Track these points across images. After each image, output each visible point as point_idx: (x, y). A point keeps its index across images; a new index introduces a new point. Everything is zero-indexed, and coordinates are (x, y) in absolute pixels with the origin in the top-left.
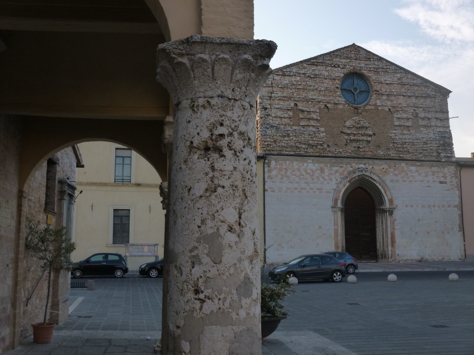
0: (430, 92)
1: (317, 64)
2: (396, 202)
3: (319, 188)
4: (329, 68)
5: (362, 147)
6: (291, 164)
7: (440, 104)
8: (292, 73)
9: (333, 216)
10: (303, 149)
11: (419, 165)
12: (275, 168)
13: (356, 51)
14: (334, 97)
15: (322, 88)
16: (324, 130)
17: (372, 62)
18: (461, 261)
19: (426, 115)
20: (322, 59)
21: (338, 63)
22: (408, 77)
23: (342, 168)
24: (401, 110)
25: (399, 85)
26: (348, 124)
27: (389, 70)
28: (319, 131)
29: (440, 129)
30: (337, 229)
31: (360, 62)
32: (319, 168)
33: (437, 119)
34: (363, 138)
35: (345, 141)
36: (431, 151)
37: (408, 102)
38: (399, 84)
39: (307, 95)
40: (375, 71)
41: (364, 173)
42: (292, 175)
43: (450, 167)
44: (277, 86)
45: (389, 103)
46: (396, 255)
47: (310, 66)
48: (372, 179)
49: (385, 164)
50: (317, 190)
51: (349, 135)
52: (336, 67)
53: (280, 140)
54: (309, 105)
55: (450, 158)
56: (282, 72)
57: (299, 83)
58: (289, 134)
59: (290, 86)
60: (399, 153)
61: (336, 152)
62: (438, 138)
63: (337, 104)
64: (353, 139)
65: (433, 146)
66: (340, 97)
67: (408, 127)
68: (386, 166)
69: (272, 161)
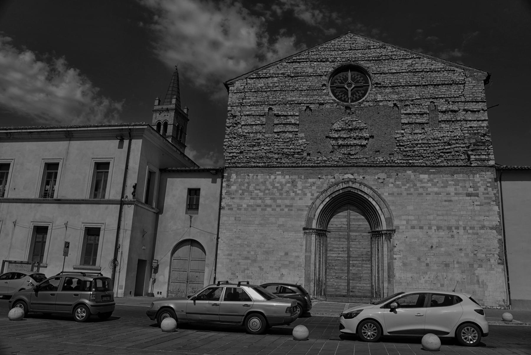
1: (300, 61)
3: (289, 204)
4: (315, 63)
5: (353, 153)
6: (255, 177)
7: (472, 91)
8: (268, 74)
10: (275, 159)
11: (434, 172)
13: (352, 40)
14: (319, 95)
15: (304, 87)
18: (502, 308)
19: (450, 107)
20: (307, 55)
21: (326, 57)
22: (424, 62)
23: (321, 180)
24: (412, 104)
25: (410, 74)
26: (336, 126)
27: (395, 56)
29: (471, 124)
30: (310, 257)
32: (290, 180)
34: (355, 142)
35: (331, 147)
36: (457, 154)
37: (423, 93)
38: (410, 71)
43: (484, 173)
44: (249, 91)
45: (395, 97)
50: (285, 207)
51: (336, 139)
53: (248, 151)
56: (256, 75)
57: (277, 85)
59: (265, 89)
60: (407, 158)
61: (319, 162)
62: (467, 136)
64: (341, 144)
65: (460, 146)
68: (383, 176)
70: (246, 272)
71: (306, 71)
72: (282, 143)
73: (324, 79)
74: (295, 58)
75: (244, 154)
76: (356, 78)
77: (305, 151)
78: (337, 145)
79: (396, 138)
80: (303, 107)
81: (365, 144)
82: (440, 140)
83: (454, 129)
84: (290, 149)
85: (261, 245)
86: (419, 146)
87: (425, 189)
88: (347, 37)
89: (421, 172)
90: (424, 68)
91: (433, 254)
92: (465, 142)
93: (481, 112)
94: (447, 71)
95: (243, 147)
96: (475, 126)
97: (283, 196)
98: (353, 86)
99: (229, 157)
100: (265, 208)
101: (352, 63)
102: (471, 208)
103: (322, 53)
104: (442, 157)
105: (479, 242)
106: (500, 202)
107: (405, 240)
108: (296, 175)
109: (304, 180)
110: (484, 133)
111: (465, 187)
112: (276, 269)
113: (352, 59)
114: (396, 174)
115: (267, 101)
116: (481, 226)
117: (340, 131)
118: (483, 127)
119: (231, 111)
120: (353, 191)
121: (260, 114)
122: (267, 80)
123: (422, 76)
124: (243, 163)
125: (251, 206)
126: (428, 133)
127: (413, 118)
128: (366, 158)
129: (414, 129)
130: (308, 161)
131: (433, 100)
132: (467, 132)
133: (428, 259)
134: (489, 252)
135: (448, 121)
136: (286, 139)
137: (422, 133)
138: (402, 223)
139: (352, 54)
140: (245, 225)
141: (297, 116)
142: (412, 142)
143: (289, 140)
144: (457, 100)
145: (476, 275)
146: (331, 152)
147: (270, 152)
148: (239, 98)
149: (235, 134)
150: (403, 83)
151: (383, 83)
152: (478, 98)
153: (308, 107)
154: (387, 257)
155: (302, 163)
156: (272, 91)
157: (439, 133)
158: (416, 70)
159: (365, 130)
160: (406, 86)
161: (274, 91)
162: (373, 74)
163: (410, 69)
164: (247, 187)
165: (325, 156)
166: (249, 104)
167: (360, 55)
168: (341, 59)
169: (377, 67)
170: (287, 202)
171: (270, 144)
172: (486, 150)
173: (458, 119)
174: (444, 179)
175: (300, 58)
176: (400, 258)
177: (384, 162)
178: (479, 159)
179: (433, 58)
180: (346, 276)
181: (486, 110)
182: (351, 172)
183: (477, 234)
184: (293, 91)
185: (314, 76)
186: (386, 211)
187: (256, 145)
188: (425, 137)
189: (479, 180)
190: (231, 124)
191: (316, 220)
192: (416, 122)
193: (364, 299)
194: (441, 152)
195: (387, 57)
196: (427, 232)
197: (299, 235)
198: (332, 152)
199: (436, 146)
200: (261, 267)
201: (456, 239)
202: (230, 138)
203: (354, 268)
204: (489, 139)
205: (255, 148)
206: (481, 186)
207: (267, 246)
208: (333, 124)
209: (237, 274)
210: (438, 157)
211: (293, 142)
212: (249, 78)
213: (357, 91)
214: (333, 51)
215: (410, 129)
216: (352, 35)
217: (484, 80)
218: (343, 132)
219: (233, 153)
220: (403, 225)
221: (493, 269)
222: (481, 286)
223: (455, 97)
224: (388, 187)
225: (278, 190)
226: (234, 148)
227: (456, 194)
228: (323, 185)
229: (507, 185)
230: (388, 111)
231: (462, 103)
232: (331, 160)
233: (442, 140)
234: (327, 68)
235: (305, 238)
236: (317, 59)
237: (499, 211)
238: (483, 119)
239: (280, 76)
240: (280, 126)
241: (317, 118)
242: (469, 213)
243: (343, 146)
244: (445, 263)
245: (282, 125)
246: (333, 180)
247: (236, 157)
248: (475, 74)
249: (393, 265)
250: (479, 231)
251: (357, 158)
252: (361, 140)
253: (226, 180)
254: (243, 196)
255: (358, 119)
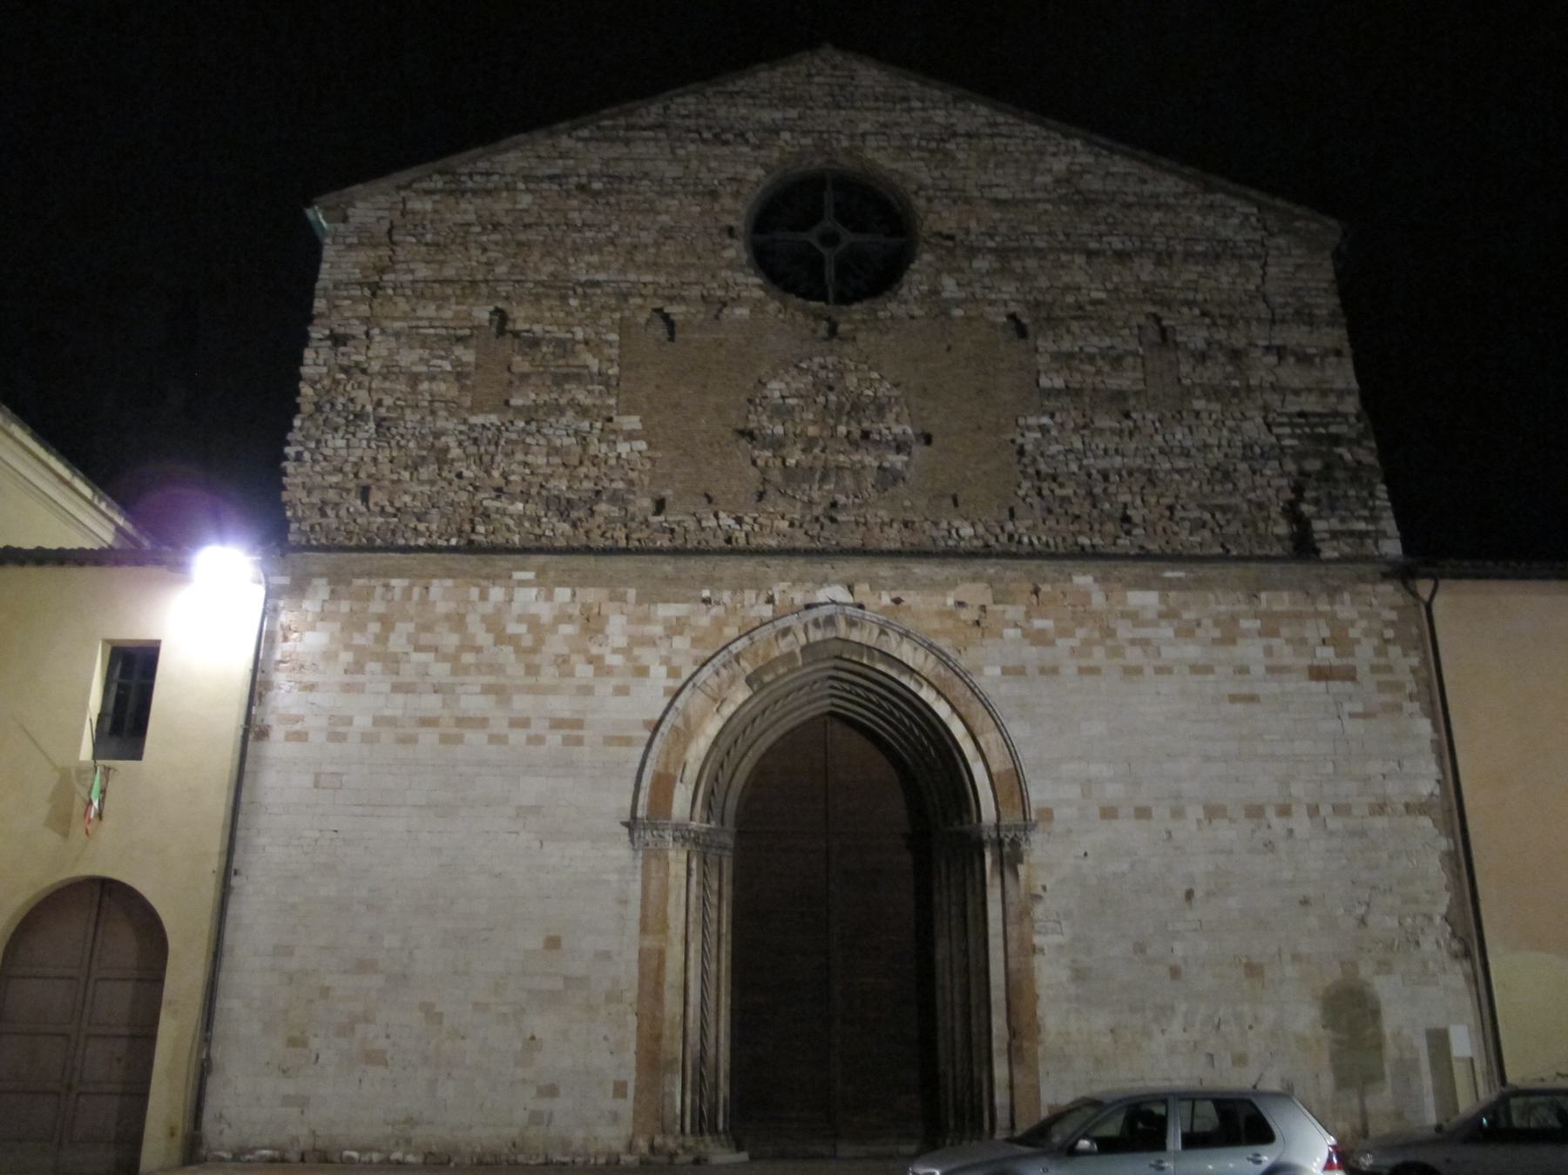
0: (1236, 233)
2: (1038, 794)
4: (692, 148)
9: (639, 877)
11: (1179, 579)
16: (639, 426)
22: (1114, 169)
25: (1064, 208)
28: (614, 431)
30: (661, 954)
31: (852, 113)
32: (575, 611)
33: (1281, 352)
39: (562, 269)
40: (932, 151)
41: (842, 630)
43: (1369, 588)
45: (1009, 289)
47: (592, 145)
48: (891, 666)
49: (975, 579)
52: (726, 143)
54: (568, 314)
55: (1369, 542)
58: (447, 450)
62: (1292, 447)
66: (741, 268)
67: (1120, 396)
68: (976, 593)
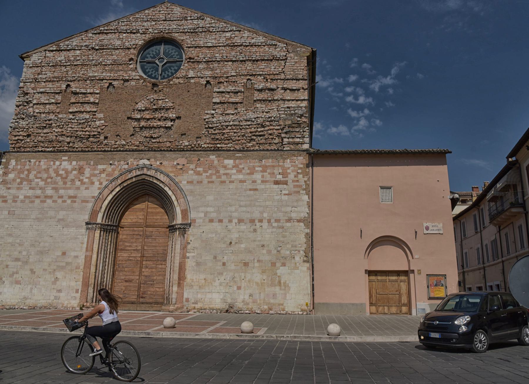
1: (107, 32)
3: (73, 195)
4: (124, 35)
5: (156, 136)
6: (37, 163)
7: (293, 68)
10: (66, 143)
11: (240, 156)
12: (13, 170)
13: (168, 10)
15: (108, 61)
17: (189, 21)
20: (116, 25)
22: (244, 35)
23: (112, 166)
24: (227, 82)
25: (227, 48)
26: (140, 106)
27: (213, 28)
29: (289, 104)
32: (77, 167)
34: (159, 124)
35: (132, 129)
37: (240, 69)
38: (228, 45)
41: (145, 171)
42: (36, 178)
43: (296, 158)
44: (47, 65)
45: (208, 73)
46: (184, 300)
48: (158, 181)
50: (68, 198)
51: (138, 120)
53: (37, 133)
56: (57, 47)
57: (78, 58)
59: (64, 63)
60: (216, 142)
61: (116, 146)
63: (127, 81)
68: (182, 161)
69: (12, 161)
70: (15, 276)
71: (113, 44)
72: (77, 124)
73: (132, 52)
74: (103, 29)
75: (32, 137)
76: (170, 52)
77: (103, 134)
78: (139, 128)
79: (205, 119)
80: (105, 84)
81: (170, 125)
82: (253, 122)
83: (270, 110)
84: (85, 131)
85: (35, 243)
86: (229, 128)
87: (229, 176)
88: (163, 6)
89: (226, 156)
90: (244, 41)
91: (231, 251)
92: (280, 124)
93: (301, 90)
94: (268, 45)
95: (32, 130)
96: (293, 106)
97: (68, 186)
98: (165, 61)
99: (14, 140)
100: (44, 199)
101: (165, 35)
102: (278, 197)
103: (134, 24)
104: (254, 140)
105: (284, 237)
106: (311, 192)
107: (201, 235)
108: (84, 160)
109: (94, 167)
110: (302, 113)
111: (274, 173)
112: (50, 272)
113: (165, 31)
114: (197, 159)
115: (65, 77)
116: (287, 218)
117: (143, 111)
118: (301, 107)
119: (23, 88)
120: (148, 179)
121: (55, 91)
122: (68, 52)
123: (241, 51)
124: (29, 147)
125: (29, 197)
126: (241, 114)
127: (226, 97)
128: (170, 142)
129: (226, 109)
130: (104, 145)
131: (250, 77)
132: (283, 112)
133: (226, 257)
134: (294, 249)
135: (264, 101)
136: (81, 120)
137: (234, 114)
138: (199, 216)
139: (166, 25)
140: (19, 220)
141: (97, 94)
142: (222, 123)
143: (84, 121)
144: (276, 77)
145: (278, 275)
146: (131, 136)
147: (63, 135)
148: (35, 73)
149: (24, 115)
150: (218, 58)
151: (196, 58)
152: (299, 76)
153: (110, 84)
154: (179, 255)
155: (97, 148)
156: (73, 65)
157: (253, 113)
158: (234, 43)
159: (171, 110)
160: (221, 61)
161: (75, 65)
162: (187, 47)
163: (228, 43)
164: (26, 175)
165: (124, 140)
166: (45, 80)
167: (175, 27)
168: (153, 31)
169: (192, 40)
170: (71, 192)
171: (63, 125)
172: (301, 132)
173: (275, 98)
174: (251, 164)
175: (108, 28)
176: (193, 257)
177: (189, 147)
178: (292, 142)
179: (254, 32)
180: (137, 279)
181: (306, 89)
182: (147, 157)
183: (283, 227)
184: (96, 65)
185: (121, 49)
186: (182, 202)
187: (47, 127)
188: (237, 119)
189: (290, 166)
190: (21, 103)
191: (103, 213)
192: (229, 101)
193: (155, 305)
194: (254, 135)
195: (204, 30)
196: (227, 226)
197: (80, 231)
198: (133, 135)
199: (248, 128)
200: (33, 269)
201: (259, 233)
202: (18, 119)
203: (147, 270)
204: (305, 120)
205: (45, 131)
206: (291, 173)
207: (42, 244)
208: (137, 103)
209: (4, 279)
210: (249, 141)
211: (89, 123)
212: (49, 51)
213: (170, 67)
214: (146, 21)
215: (222, 109)
216: (169, 5)
217: (307, 57)
218: (147, 112)
219: (19, 136)
220: (200, 218)
221: (297, 268)
222: (283, 288)
223: (275, 75)
224: (187, 174)
225: (62, 178)
226: (21, 130)
227: (263, 182)
228: (114, 172)
229: (319, 171)
230: (200, 89)
231: (281, 81)
232: (131, 144)
233: (255, 122)
234: (137, 41)
235: (87, 235)
236: (126, 30)
237: (308, 200)
238: (302, 98)
239: (83, 48)
240: (77, 105)
241: (120, 96)
242: (276, 203)
243: (146, 128)
244: (244, 261)
245: (80, 105)
246: (126, 167)
247: (22, 140)
248: (298, 49)
249: (185, 265)
250: (285, 224)
251: (159, 142)
252: (166, 121)
253: (3, 167)
254: (22, 186)
255: (164, 98)
